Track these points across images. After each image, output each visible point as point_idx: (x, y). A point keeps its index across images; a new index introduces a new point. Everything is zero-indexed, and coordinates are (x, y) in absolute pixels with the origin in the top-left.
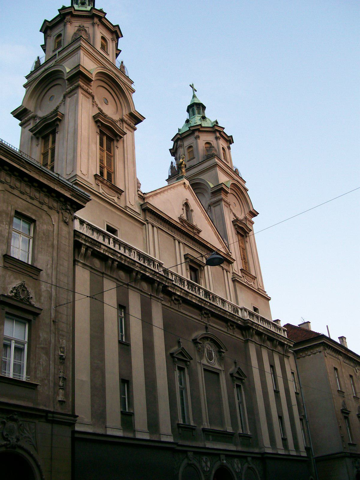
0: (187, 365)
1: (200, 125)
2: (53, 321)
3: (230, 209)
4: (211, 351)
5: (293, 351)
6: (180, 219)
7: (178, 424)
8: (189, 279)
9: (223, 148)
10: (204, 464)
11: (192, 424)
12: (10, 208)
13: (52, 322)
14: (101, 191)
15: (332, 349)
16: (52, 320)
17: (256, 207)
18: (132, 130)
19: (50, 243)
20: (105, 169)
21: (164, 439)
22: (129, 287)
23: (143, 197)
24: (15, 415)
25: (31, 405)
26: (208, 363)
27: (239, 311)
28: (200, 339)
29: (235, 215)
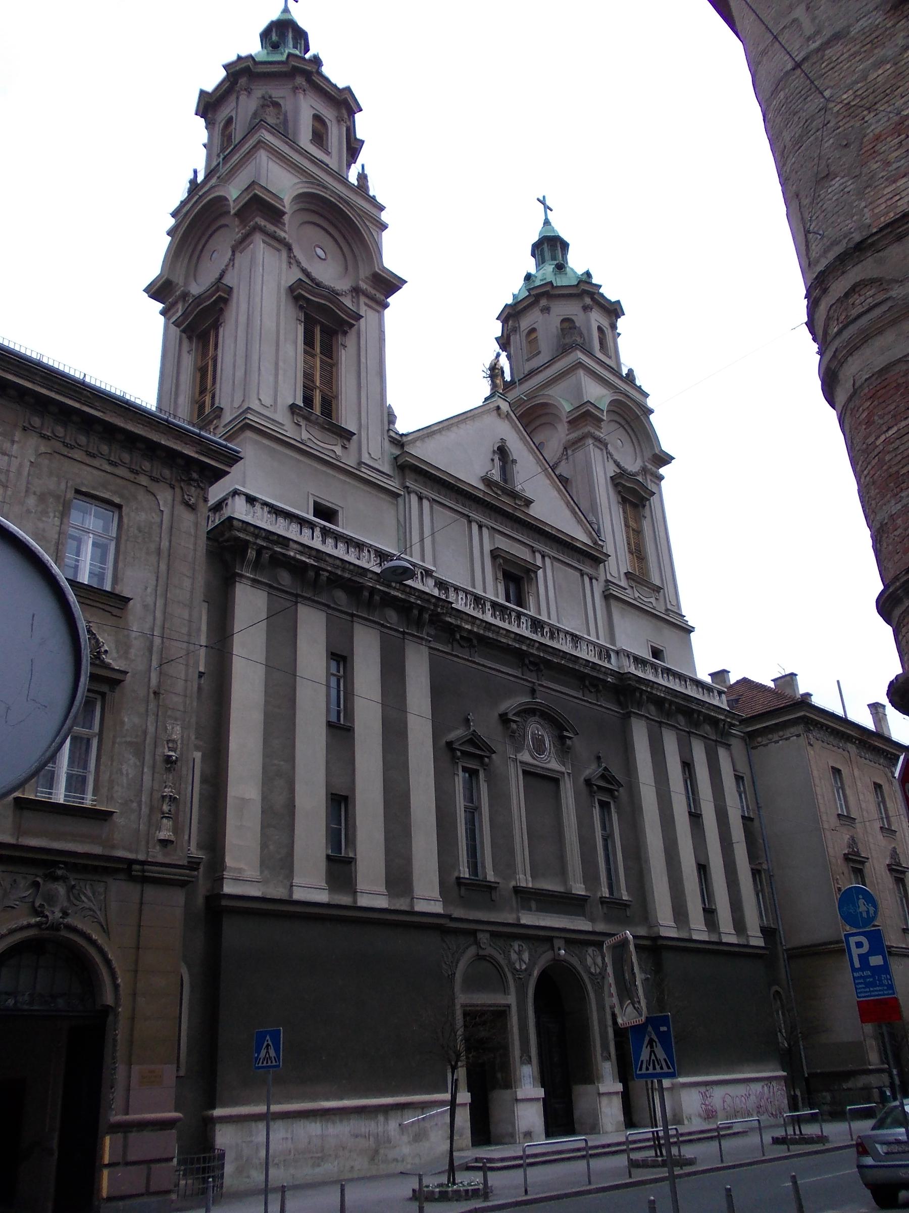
0: (482, 764)
1: (551, 283)
2: (155, 693)
3: (608, 453)
4: (542, 736)
5: (744, 733)
6: (487, 481)
7: (458, 878)
8: (501, 600)
9: (600, 329)
10: (514, 956)
11: (491, 877)
12: (63, 486)
13: (152, 695)
14: (305, 435)
15: (829, 730)
16: (151, 691)
17: (667, 445)
18: (379, 308)
19: (153, 547)
20: (318, 391)
21: (421, 907)
22: (355, 618)
23: (400, 441)
24: (61, 868)
25: (97, 850)
26: (534, 758)
27: (613, 655)
28: (517, 714)
29: (618, 465)
